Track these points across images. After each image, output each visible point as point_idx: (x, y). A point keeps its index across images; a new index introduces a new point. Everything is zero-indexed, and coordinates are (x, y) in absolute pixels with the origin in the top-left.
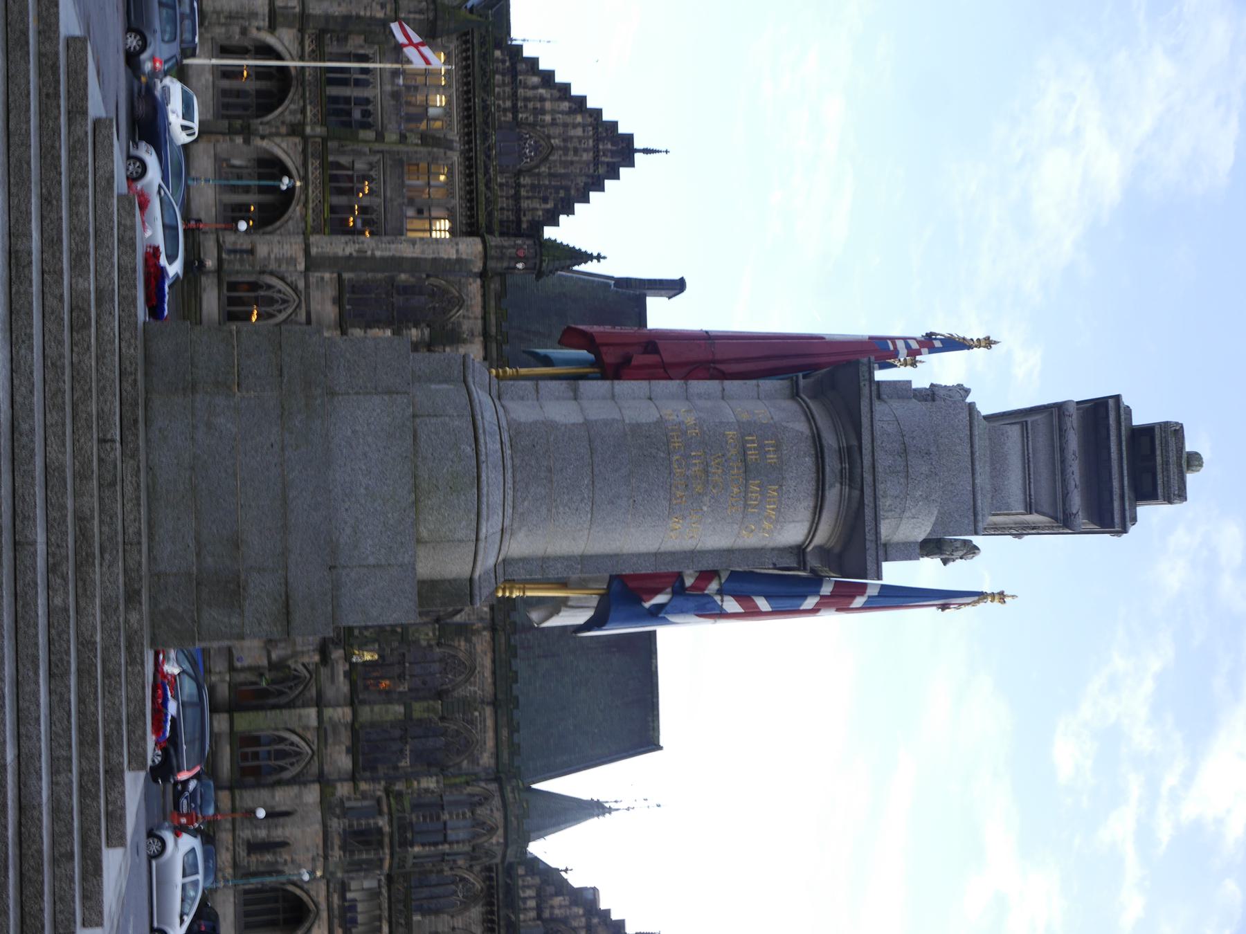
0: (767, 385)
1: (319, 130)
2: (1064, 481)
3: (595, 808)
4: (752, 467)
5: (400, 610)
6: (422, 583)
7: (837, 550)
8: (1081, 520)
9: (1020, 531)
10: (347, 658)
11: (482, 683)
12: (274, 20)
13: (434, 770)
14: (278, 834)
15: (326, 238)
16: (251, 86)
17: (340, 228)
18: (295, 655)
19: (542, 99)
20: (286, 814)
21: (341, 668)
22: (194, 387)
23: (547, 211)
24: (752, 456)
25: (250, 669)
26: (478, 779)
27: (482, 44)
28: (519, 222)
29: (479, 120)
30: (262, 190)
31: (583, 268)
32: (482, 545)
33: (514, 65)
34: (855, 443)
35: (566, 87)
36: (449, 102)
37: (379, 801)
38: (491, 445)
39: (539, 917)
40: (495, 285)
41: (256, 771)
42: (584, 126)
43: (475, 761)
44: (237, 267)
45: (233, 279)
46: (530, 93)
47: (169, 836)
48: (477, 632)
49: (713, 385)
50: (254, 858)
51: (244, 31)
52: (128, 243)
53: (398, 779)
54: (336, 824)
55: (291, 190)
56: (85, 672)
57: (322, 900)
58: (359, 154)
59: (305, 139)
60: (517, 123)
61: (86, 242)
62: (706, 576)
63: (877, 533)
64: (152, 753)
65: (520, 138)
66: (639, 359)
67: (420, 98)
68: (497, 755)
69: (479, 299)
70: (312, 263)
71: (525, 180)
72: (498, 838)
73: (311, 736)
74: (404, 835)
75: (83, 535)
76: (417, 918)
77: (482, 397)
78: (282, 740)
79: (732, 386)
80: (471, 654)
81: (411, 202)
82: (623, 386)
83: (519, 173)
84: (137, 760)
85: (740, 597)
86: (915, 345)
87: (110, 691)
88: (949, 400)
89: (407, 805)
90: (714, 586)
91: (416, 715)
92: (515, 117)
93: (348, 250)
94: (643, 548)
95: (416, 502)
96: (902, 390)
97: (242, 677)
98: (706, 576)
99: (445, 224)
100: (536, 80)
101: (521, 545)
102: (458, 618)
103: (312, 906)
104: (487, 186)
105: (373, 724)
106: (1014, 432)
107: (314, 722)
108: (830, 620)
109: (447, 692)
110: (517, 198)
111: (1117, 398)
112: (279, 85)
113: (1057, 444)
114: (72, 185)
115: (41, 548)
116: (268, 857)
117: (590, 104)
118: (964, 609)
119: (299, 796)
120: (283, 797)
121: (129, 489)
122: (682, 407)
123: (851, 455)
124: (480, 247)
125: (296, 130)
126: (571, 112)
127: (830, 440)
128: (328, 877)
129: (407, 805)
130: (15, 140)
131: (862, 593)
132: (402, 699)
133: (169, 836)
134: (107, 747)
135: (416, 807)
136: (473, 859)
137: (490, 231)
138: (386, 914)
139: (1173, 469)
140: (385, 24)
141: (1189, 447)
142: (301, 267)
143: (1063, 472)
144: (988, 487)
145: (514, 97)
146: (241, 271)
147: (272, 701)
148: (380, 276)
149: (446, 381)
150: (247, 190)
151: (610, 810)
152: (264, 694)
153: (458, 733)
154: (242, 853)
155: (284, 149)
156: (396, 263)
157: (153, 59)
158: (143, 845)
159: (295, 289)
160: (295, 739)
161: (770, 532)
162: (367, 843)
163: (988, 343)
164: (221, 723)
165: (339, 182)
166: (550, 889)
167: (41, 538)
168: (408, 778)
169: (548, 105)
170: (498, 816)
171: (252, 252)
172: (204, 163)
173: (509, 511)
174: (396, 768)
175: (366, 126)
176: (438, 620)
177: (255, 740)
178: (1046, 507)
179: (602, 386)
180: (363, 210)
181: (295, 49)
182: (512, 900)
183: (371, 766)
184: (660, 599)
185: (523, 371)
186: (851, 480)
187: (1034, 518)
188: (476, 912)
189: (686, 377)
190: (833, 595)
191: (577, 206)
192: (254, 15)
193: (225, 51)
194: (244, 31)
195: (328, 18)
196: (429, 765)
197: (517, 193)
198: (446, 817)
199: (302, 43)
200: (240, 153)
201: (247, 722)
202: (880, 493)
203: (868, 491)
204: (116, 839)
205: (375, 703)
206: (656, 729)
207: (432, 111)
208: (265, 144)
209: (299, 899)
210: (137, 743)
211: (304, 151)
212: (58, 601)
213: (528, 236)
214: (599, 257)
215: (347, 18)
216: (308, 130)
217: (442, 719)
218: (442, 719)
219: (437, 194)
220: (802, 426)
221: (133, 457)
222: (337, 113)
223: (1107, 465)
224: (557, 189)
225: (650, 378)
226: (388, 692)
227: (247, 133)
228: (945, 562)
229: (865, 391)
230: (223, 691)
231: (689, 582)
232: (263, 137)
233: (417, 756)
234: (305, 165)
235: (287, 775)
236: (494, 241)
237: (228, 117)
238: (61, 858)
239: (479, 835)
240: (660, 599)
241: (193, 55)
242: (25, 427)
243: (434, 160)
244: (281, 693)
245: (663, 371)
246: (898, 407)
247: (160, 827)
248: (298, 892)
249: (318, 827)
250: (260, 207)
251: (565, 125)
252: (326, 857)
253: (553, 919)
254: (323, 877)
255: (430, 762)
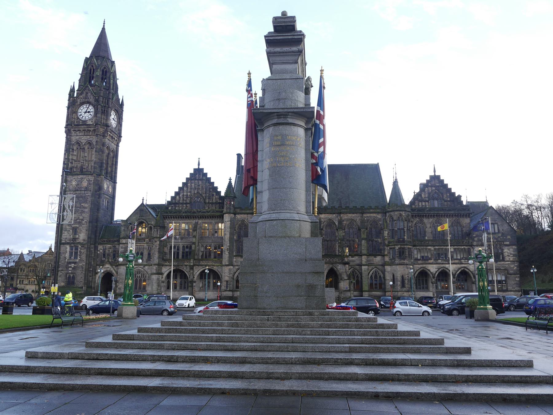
0: (259, 138)
1: (192, 261)
2: (289, 52)
3: (395, 183)
4: (282, 143)
5: (319, 241)
6: (311, 236)
7: (306, 119)
8: (300, 47)
9: (304, 64)
10: (347, 257)
11: (356, 217)
12: (160, 273)
13: (382, 232)
14: (399, 278)
15: (223, 260)
16: (179, 281)
17: (221, 256)
18: (346, 272)
19: (183, 195)
20: (393, 276)
21: (350, 258)
22: (256, 296)
23: (216, 195)
24: (279, 143)
25: (350, 285)
26: (385, 218)
27: (167, 213)
28: (219, 203)
29: (189, 214)
30: (209, 278)
31: (233, 184)
32: (301, 219)
33: (173, 204)
34: (276, 114)
35: (180, 188)
36: (184, 223)
37: (390, 248)
38: (274, 216)
39: (428, 201)
40: (238, 211)
41: (381, 285)
42: (191, 183)
43: (380, 220)
44: (231, 286)
45: (235, 287)
46: (181, 199)
47: (395, 310)
48: (341, 218)
49: (259, 154)
50: (406, 286)
51: (163, 282)
52: (216, 312)
53: (384, 242)
54: (397, 261)
55: (209, 269)
56: (329, 326)
57: (420, 266)
58: (199, 250)
59: (194, 265)
60: (190, 203)
61: (215, 323)
62: (313, 156)
63: (301, 108)
64: (371, 315)
65: (195, 202)
66: (252, 174)
67: (183, 231)
68: (378, 213)
69: (242, 215)
70: (231, 264)
71: (207, 201)
72: (403, 213)
73: (370, 268)
74: (401, 241)
75: (292, 326)
76: (426, 238)
77: (261, 218)
78: (371, 276)
79: (260, 148)
80: (347, 220)
81: (213, 235)
82: (259, 179)
83: (205, 203)
84: (355, 314)
85: (319, 147)
86: (250, 95)
87: (335, 320)
88: (265, 83)
89: (392, 240)
90: (316, 154)
91: (365, 237)
92: (189, 203)
93: (227, 253)
94: (304, 174)
95: (289, 237)
96: (262, 99)
97: (352, 288)
98: (313, 156)
99: (220, 225)
100: (177, 197)
101: (302, 208)
102: (337, 224)
103: (422, 269)
104: (208, 212)
105: (368, 250)
106: (274, 67)
107: (367, 267)
108: (326, 121)
109: (358, 227)
110: (212, 203)
111: (265, 37)
112: (178, 272)
113: (278, 54)
114: (200, 326)
115: (294, 336)
116: (406, 281)
117: (185, 181)
118: (325, 82)
119: (388, 272)
120: (388, 277)
121: (282, 314)
122: (265, 162)
123: (279, 115)
124: (227, 215)
125: (192, 268)
126: (187, 187)
127: (275, 121)
128: (413, 264)
129: (392, 240)
130: (187, 339)
131: (319, 111)
132: (360, 241)
133: (395, 310)
134: (350, 321)
135: (393, 238)
136: (409, 221)
137: (222, 211)
138: (425, 247)
139: (286, 20)
140: (161, 241)
141: (280, 15)
142: (232, 267)
143: (286, 53)
144: (290, 74)
145: (182, 204)
146: (233, 285)
147: (360, 279)
148: (235, 244)
149: (256, 228)
150: (209, 282)
151: (396, 179)
152: (357, 282)
153: (371, 224)
154: (404, 289)
155: (197, 271)
156: (231, 239)
157: (170, 308)
158: (397, 317)
159: (238, 269)
160: (371, 272)
161: (300, 138)
162: (403, 252)
163: (249, 74)
164: (366, 294)
165: (207, 256)
166: (420, 198)
167: (292, 336)
168: (384, 240)
169: (185, 194)
170: (396, 213)
171: (227, 281)
172: (201, 295)
173: (292, 211)
174: (381, 243)
175: (191, 247)
176: (337, 230)
177: (371, 285)
178: (296, 58)
179: (259, 185)
180: (215, 249)
181: (168, 268)
182: (422, 209)
183: (380, 250)
184: (319, 169)
185: (255, 206)
186: (286, 115)
187: (299, 61)
188: (425, 220)
189: (257, 161)
190: (320, 120)
191: (215, 186)
192: (158, 279)
193: (168, 288)
194: (163, 282)
195: (159, 258)
196: (380, 233)
197: (211, 203)
198: (396, 229)
199: (166, 265)
200: (198, 284)
201: (366, 287)
202: (290, 107)
203: (289, 110)
204: (395, 326)
205: (361, 249)
206: (372, 165)
207: (187, 228)
208: (196, 277)
209: (419, 273)
210: (350, 314)
211: (198, 265)
212: (309, 333)
213: (224, 200)
214: (230, 179)
215: (159, 252)
216: (192, 264)
217: (367, 229)
218: (367, 229)
219: (211, 227)
220: (271, 129)
221: (273, 313)
222: (187, 255)
223: (285, 39)
224: (210, 191)
225: (257, 171)
226: (358, 245)
227: (192, 282)
228: (312, 86)
229: (261, 111)
230: (356, 293)
231: (314, 161)
232: (194, 277)
233: (377, 237)
234: (202, 265)
235: (382, 276)
236: (225, 210)
237: (188, 288)
238: (377, 334)
239: (402, 219)
240: (319, 169)
241: (170, 297)
242: (262, 339)
243: (201, 227)
244: (357, 277)
245: (255, 167)
246: (266, 101)
247: (393, 312)
248: (417, 273)
249: (398, 267)
250: (214, 279)
251: (191, 189)
252: (407, 265)
253: (429, 197)
254: (413, 266)
255: (379, 233)
